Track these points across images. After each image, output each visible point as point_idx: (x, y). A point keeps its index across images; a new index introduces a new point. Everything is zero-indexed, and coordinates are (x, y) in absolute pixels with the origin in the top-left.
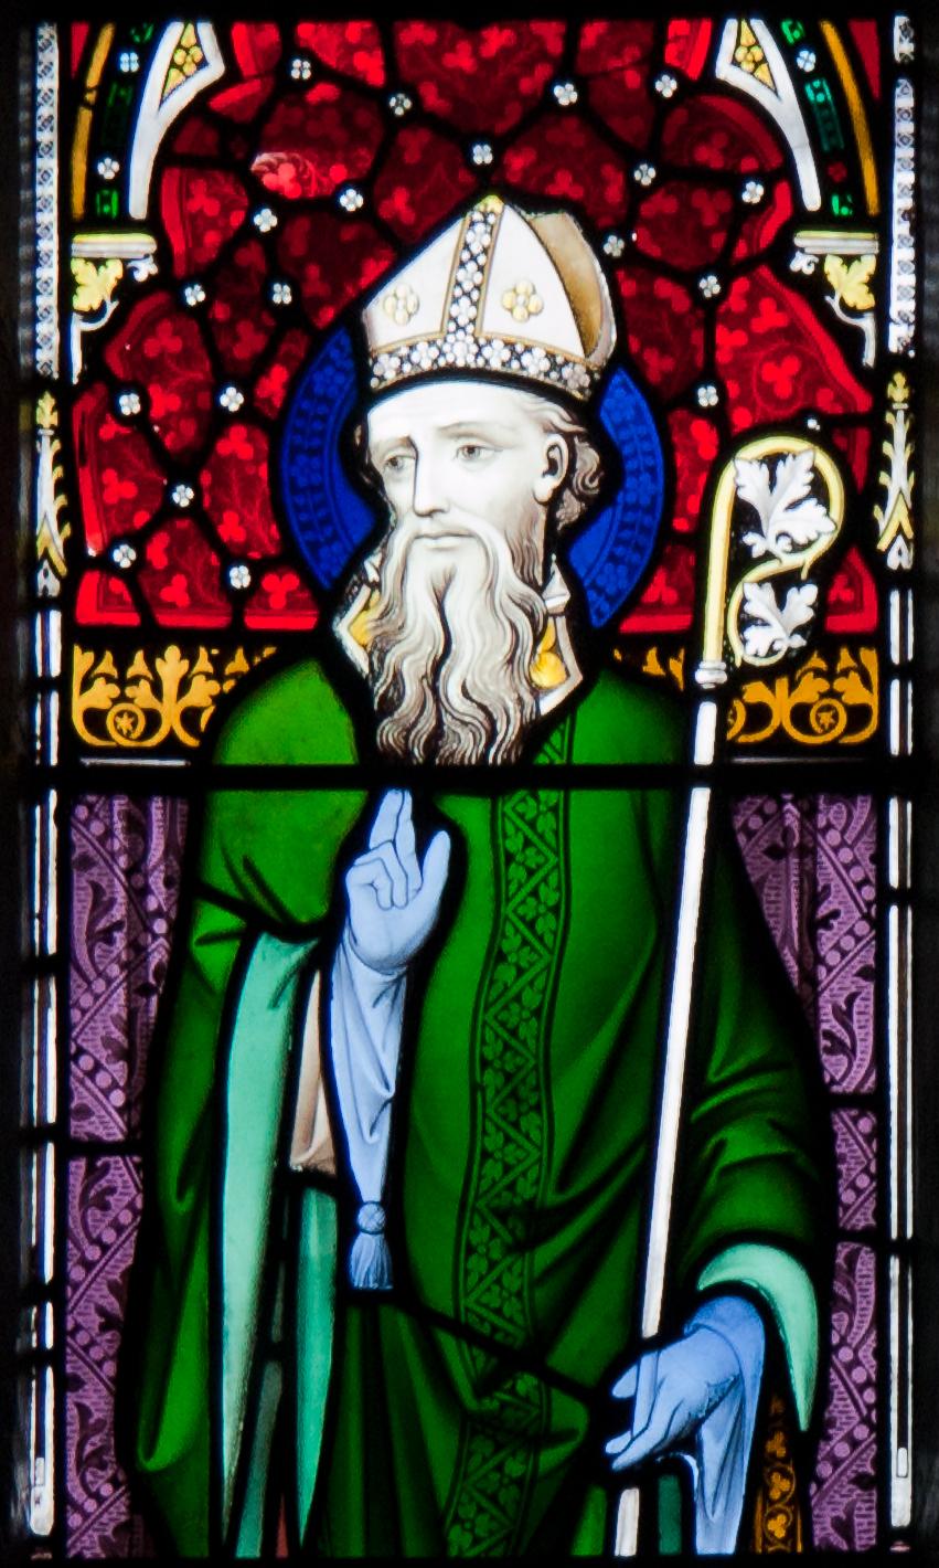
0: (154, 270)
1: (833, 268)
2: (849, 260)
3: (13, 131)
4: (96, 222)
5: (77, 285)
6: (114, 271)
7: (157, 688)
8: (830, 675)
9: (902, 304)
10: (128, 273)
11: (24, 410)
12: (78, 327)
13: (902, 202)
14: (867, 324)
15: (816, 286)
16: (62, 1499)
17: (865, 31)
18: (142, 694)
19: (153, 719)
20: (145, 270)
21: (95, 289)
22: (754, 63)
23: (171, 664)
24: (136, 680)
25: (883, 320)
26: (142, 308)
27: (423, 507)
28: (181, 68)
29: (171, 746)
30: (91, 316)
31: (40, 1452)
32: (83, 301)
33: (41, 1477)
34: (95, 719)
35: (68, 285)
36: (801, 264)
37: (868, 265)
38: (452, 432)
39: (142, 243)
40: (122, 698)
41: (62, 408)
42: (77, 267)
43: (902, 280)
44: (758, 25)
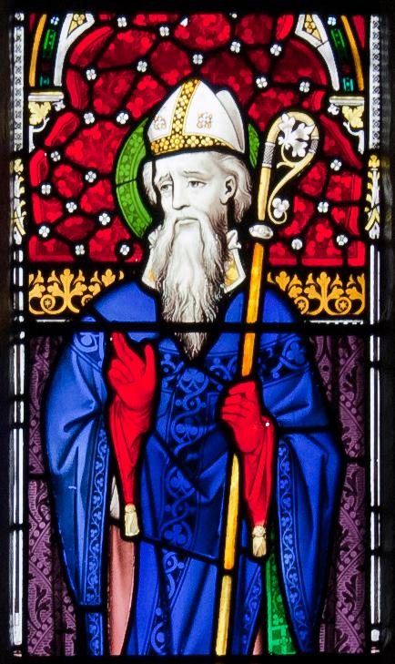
0: (63, 107)
1: (347, 112)
2: (353, 107)
3: (7, 53)
4: (39, 88)
5: (31, 114)
6: (47, 107)
7: (61, 287)
8: (344, 288)
9: (374, 129)
10: (53, 107)
11: (11, 164)
12: (32, 130)
13: (374, 84)
14: (361, 134)
15: (340, 118)
16: (25, 632)
17: (358, 19)
18: (54, 289)
19: (59, 301)
20: (60, 107)
21: (39, 115)
22: (312, 30)
23: (67, 276)
24: (52, 283)
25: (366, 128)
26: (61, 121)
27: (178, 206)
28: (74, 27)
29: (67, 313)
30: (38, 126)
31: (17, 611)
32: (34, 120)
33: (17, 619)
34: (36, 303)
35: (27, 114)
36: (333, 110)
37: (361, 109)
38: (187, 174)
39: (60, 95)
40: (46, 293)
41: (25, 163)
42: (32, 107)
43: (374, 118)
44: (315, 17)
